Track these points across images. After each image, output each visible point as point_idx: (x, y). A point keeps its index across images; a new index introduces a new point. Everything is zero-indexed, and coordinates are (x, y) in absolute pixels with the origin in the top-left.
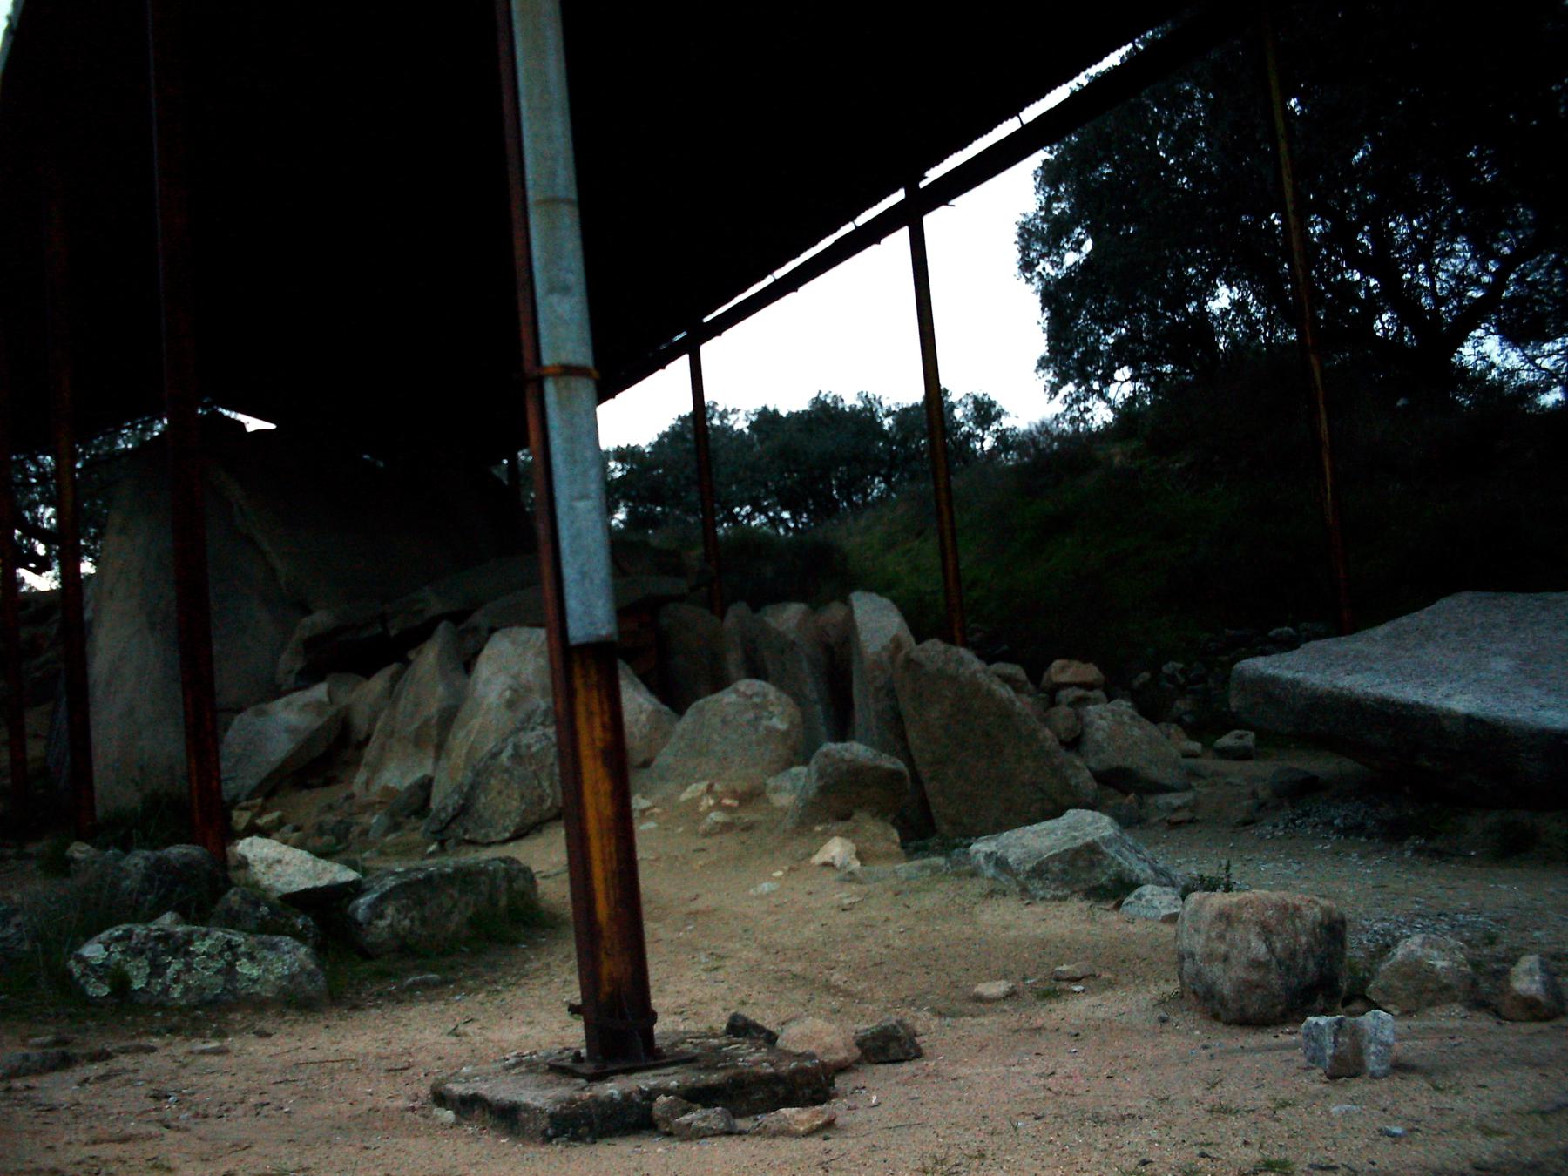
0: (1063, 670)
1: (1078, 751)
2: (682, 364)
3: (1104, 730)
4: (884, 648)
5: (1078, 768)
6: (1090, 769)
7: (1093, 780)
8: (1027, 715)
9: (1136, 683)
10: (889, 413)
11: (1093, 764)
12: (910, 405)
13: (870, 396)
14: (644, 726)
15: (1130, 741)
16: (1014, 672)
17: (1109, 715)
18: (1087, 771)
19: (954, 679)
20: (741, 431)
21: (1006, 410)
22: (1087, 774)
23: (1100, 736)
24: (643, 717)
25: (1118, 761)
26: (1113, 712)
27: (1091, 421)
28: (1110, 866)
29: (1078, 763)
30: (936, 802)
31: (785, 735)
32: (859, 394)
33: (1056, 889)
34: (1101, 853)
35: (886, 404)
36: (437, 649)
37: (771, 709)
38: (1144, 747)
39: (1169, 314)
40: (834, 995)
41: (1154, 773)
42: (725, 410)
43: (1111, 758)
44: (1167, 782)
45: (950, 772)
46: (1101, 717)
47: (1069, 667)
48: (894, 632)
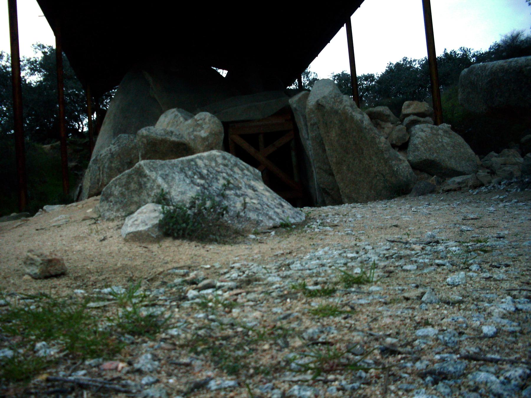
0: (408, 106)
3: (421, 138)
5: (400, 160)
6: (409, 161)
7: (411, 167)
8: (371, 129)
9: (523, 140)
10: (474, 56)
11: (410, 158)
12: (484, 52)
13: (465, 49)
16: (382, 110)
19: (336, 112)
20: (417, 69)
22: (407, 163)
23: (294, 106)
25: (426, 156)
28: (152, 188)
29: (401, 157)
32: (461, 48)
33: (118, 210)
34: (145, 176)
35: (472, 52)
40: (391, 300)
41: (452, 164)
42: (411, 61)
43: (423, 154)
44: (460, 169)
47: (412, 104)
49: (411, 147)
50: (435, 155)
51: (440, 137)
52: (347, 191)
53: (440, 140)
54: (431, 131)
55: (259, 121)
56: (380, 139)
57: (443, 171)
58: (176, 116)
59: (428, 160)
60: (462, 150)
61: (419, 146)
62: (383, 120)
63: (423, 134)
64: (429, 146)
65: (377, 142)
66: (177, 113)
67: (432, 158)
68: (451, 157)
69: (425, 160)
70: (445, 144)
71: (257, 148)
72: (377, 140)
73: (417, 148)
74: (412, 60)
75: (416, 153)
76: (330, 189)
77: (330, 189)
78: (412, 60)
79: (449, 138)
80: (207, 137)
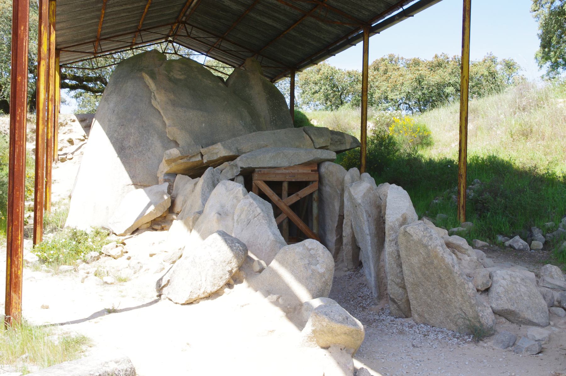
1: (488, 294)
2: (360, 45)
4: (397, 220)
5: (485, 306)
11: (494, 306)
14: (268, 247)
15: (518, 294)
17: (507, 277)
18: (490, 309)
19: (426, 246)
21: (522, 67)
22: (490, 310)
23: (500, 290)
24: (269, 243)
26: (511, 275)
27: (497, 167)
30: (413, 303)
31: (322, 275)
36: (203, 181)
37: (318, 259)
38: (526, 298)
39: (276, 116)
41: (528, 315)
45: (421, 290)
46: (504, 279)
48: (404, 211)
49: (493, 293)
50: (516, 305)
51: (517, 285)
52: (419, 309)
53: (519, 289)
54: (511, 278)
55: (286, 168)
56: (468, 284)
57: (520, 320)
58: (251, 204)
59: (510, 310)
60: (537, 301)
61: (502, 296)
62: (461, 252)
63: (504, 283)
64: (510, 296)
65: (466, 287)
66: (252, 201)
67: (513, 308)
68: (528, 308)
69: (507, 310)
70: (522, 294)
71: (280, 195)
72: (466, 286)
73: (500, 297)
74: (400, 57)
75: (499, 302)
76: (398, 300)
77: (398, 300)
78: (400, 57)
79: (525, 286)
80: (324, 273)
